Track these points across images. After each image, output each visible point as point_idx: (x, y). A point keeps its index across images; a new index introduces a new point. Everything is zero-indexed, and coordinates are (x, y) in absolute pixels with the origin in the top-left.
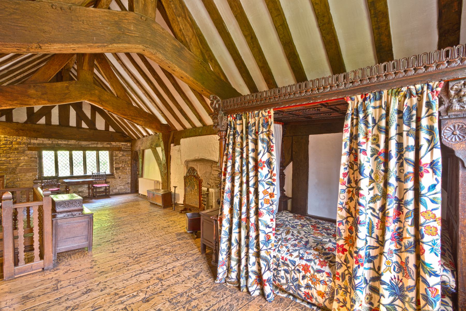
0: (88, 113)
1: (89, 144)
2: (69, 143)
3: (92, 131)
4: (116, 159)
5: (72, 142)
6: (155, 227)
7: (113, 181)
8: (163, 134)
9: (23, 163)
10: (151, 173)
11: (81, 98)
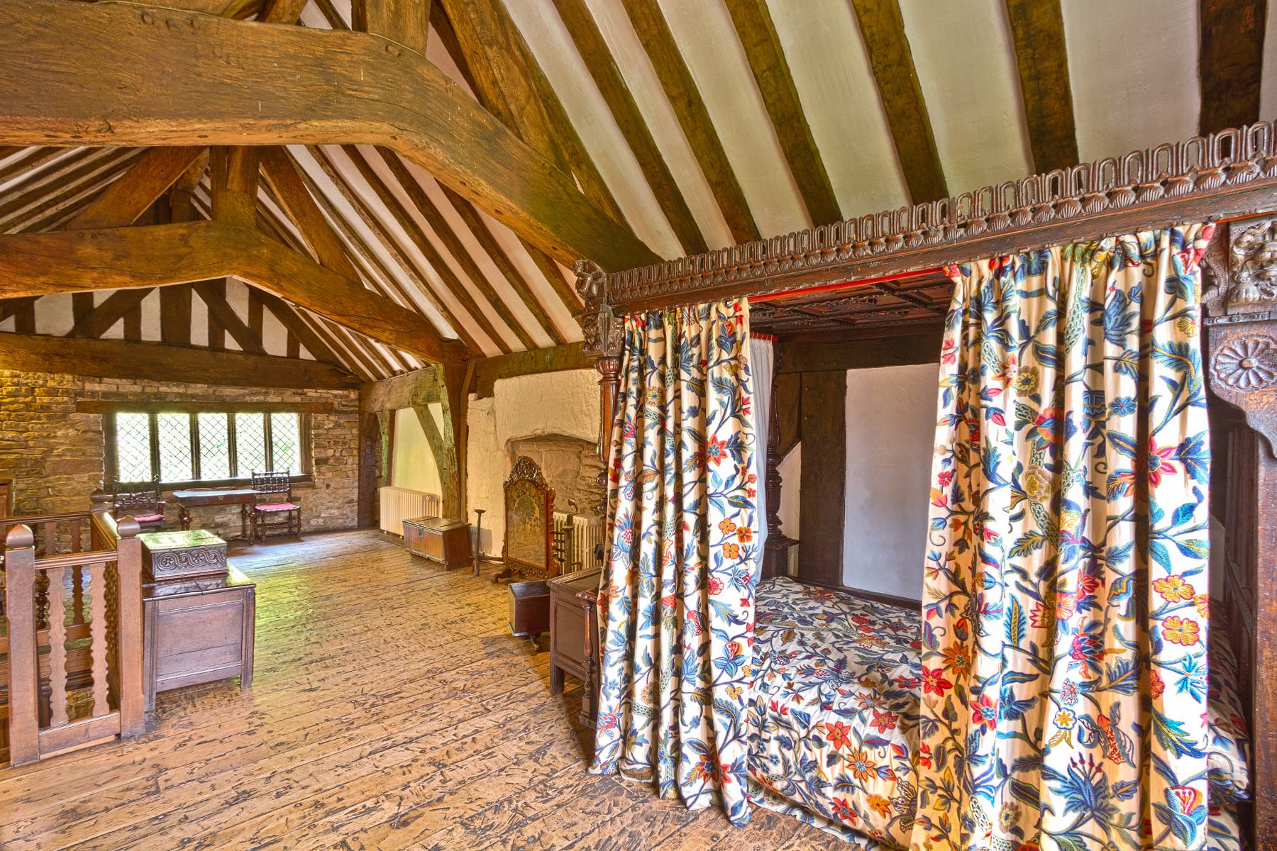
0: (241, 309)
1: (244, 395)
2: (189, 392)
5: (199, 389)
8: (446, 368)
9: (64, 447)
10: (414, 474)
11: (221, 269)
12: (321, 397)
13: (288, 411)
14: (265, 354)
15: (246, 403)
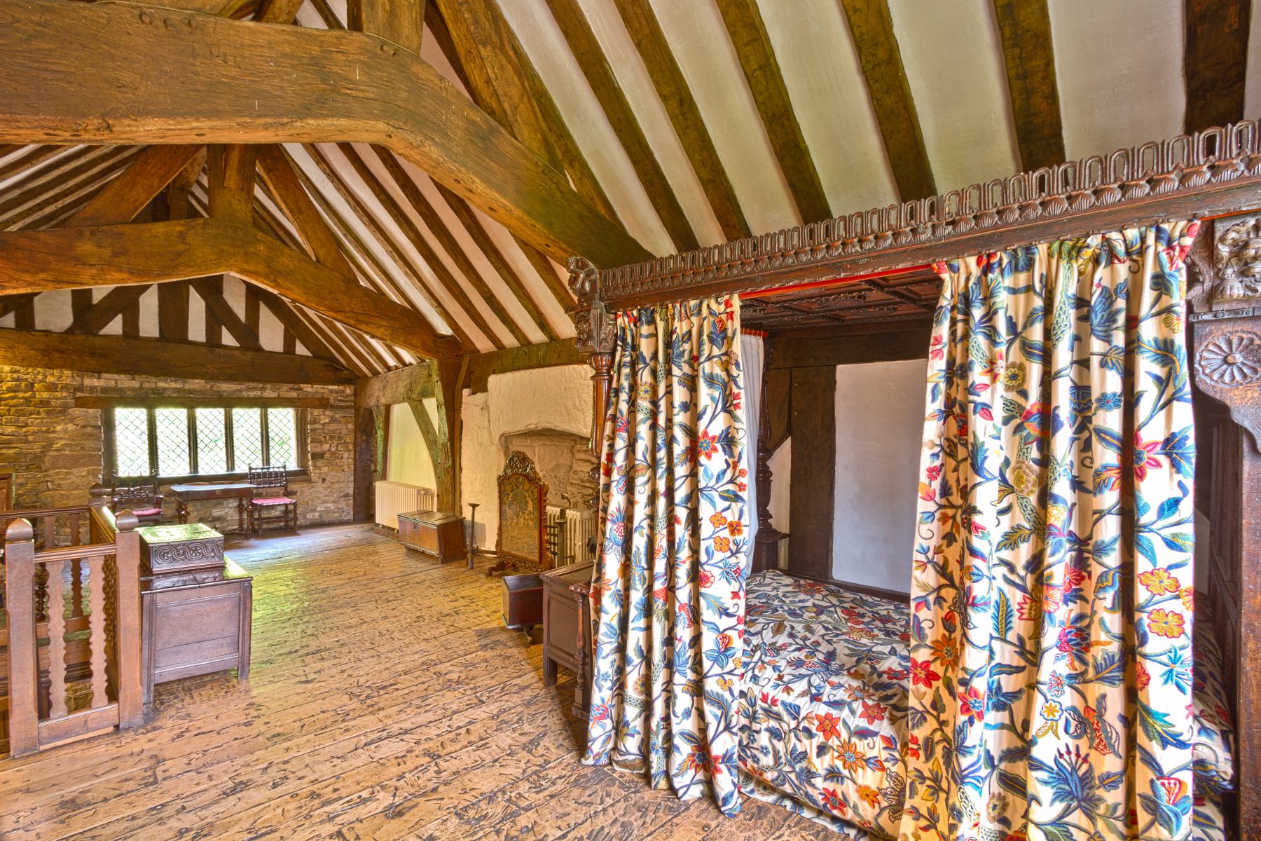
0: (238, 306)
1: (240, 391)
2: (187, 387)
3: (250, 354)
4: (313, 430)
5: (196, 384)
6: (418, 614)
7: (306, 490)
8: (440, 363)
9: (63, 442)
10: (409, 469)
11: (218, 266)
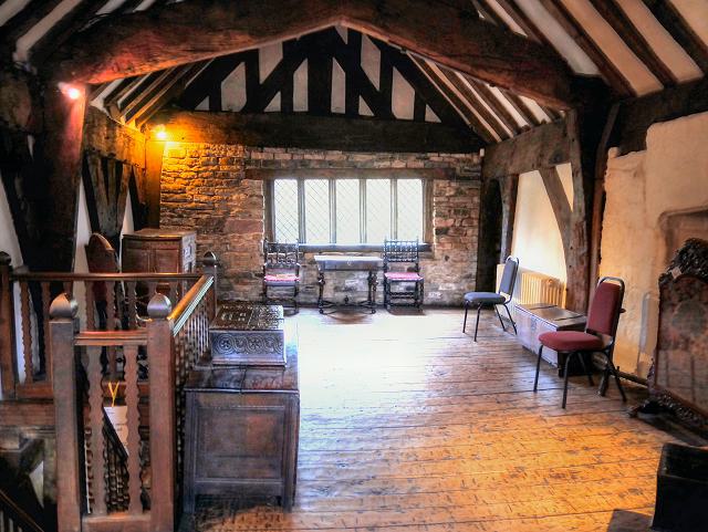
0: (374, 75)
1: (372, 161)
2: (327, 159)
3: (381, 125)
4: (438, 203)
5: (335, 155)
6: (519, 462)
7: (429, 266)
8: (579, 117)
9: (237, 210)
10: (538, 249)
11: (328, 16)
12: (443, 162)
13: (384, 177)
14: (395, 118)
15: (374, 169)
